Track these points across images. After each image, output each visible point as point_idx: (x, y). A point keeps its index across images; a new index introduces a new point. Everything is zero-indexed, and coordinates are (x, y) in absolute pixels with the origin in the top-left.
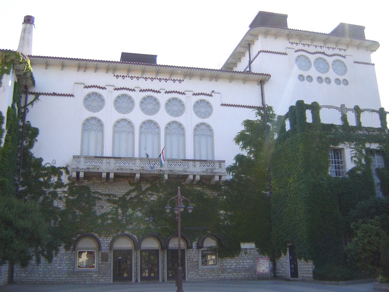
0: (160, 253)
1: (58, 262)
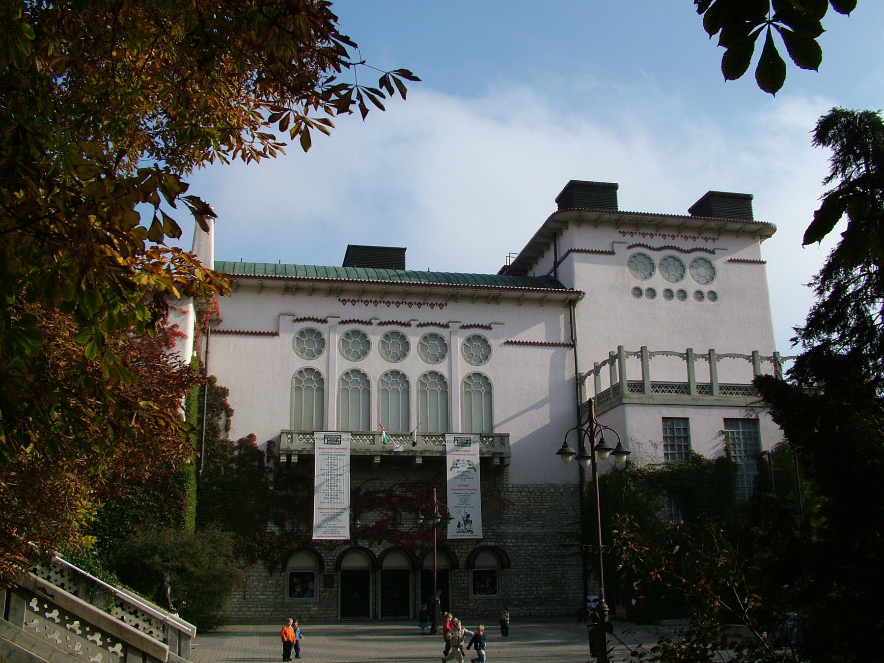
1: (260, 589)
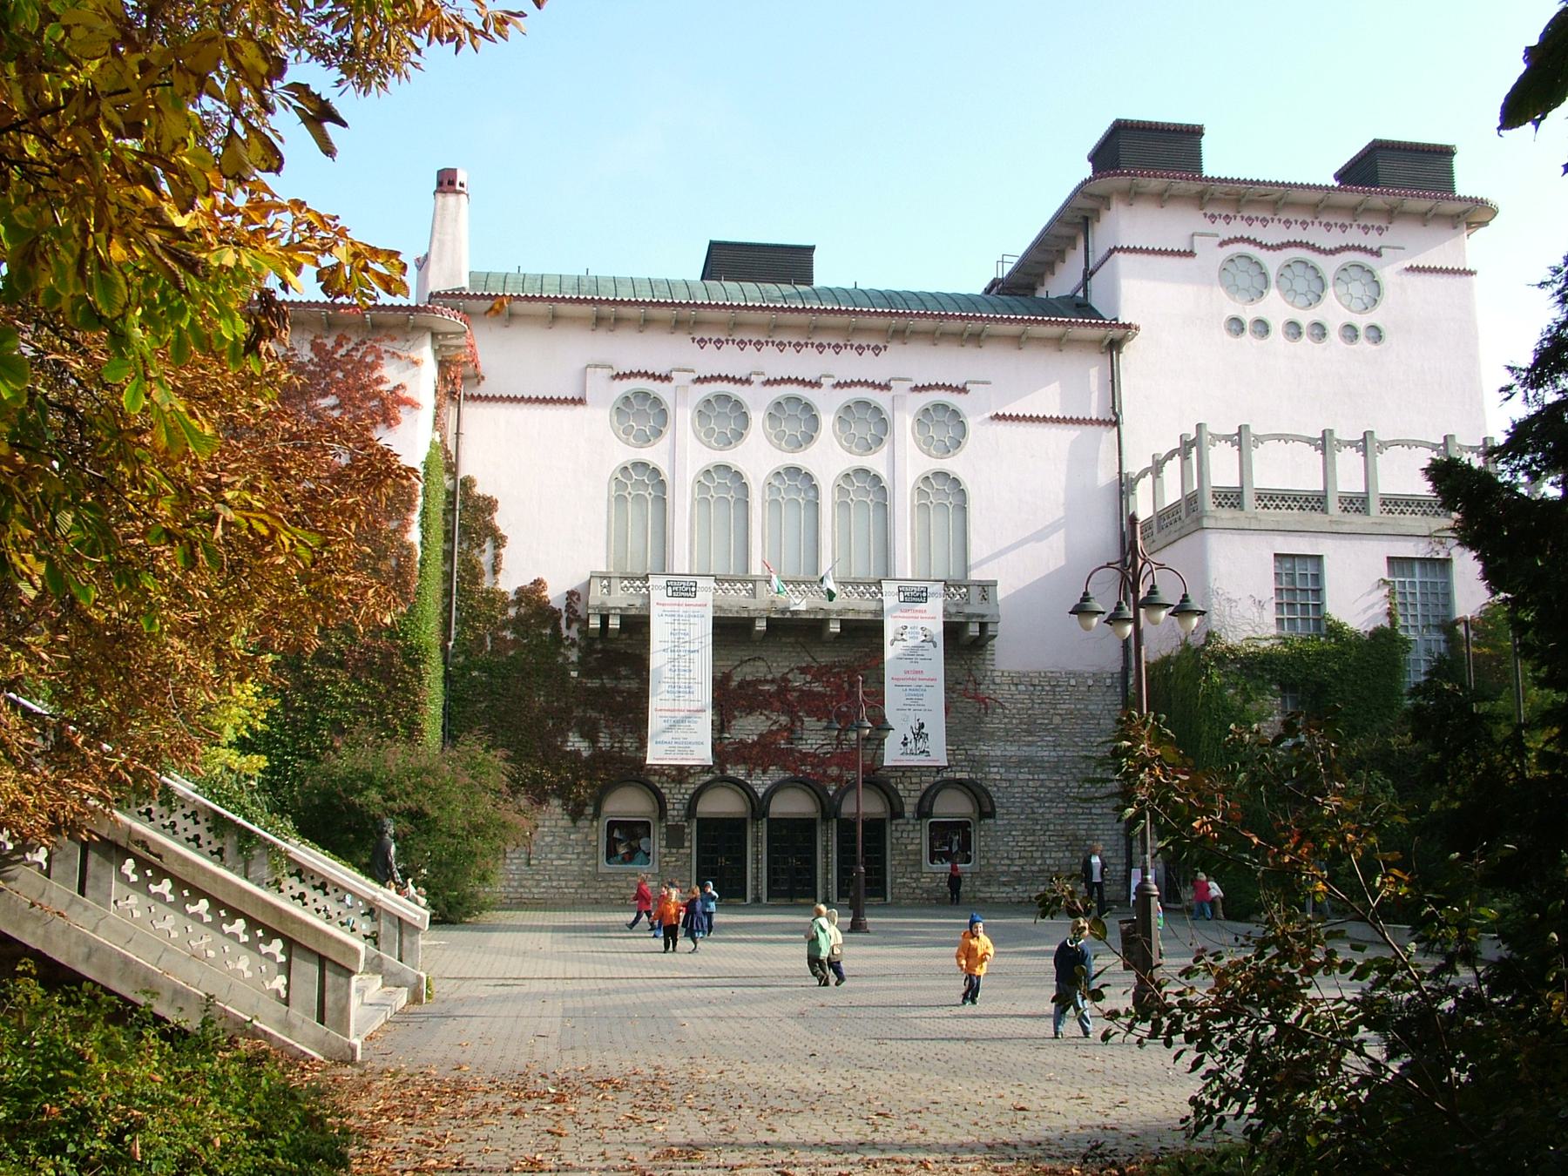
0: (819, 829)
1: (556, 849)
